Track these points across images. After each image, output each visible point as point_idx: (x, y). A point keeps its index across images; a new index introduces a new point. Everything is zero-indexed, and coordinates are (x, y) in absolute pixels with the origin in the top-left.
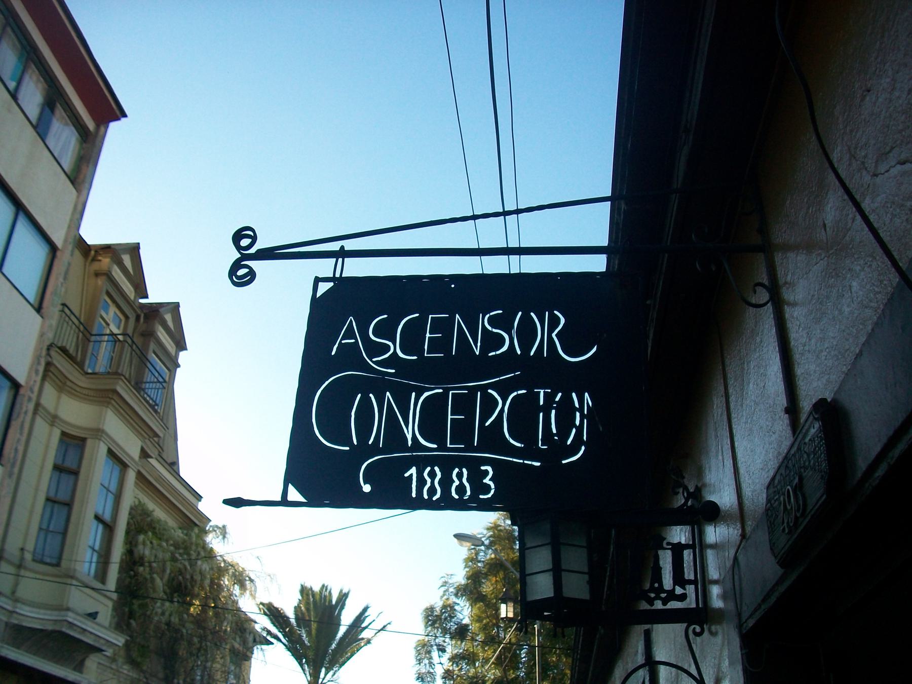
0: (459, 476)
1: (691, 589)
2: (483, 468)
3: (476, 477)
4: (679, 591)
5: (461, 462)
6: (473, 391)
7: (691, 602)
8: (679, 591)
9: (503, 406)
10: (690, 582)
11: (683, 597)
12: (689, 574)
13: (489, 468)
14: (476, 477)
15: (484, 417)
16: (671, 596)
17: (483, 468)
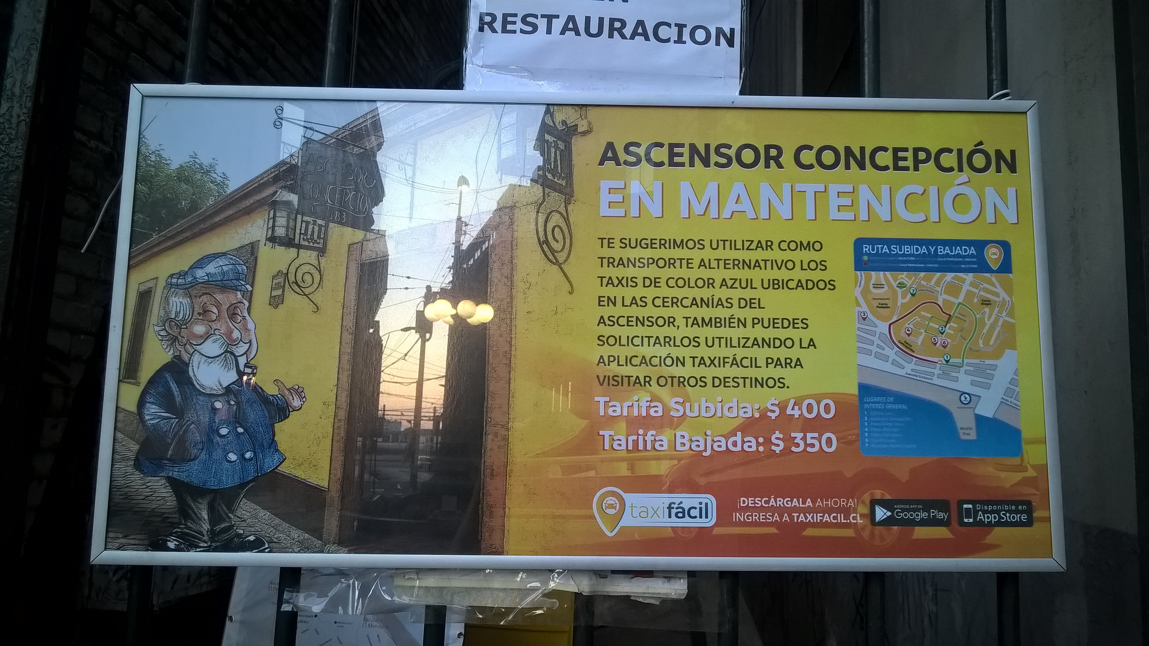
4: (318, 241)
7: (321, 246)
8: (318, 241)
11: (319, 243)
12: (322, 236)
16: (316, 242)
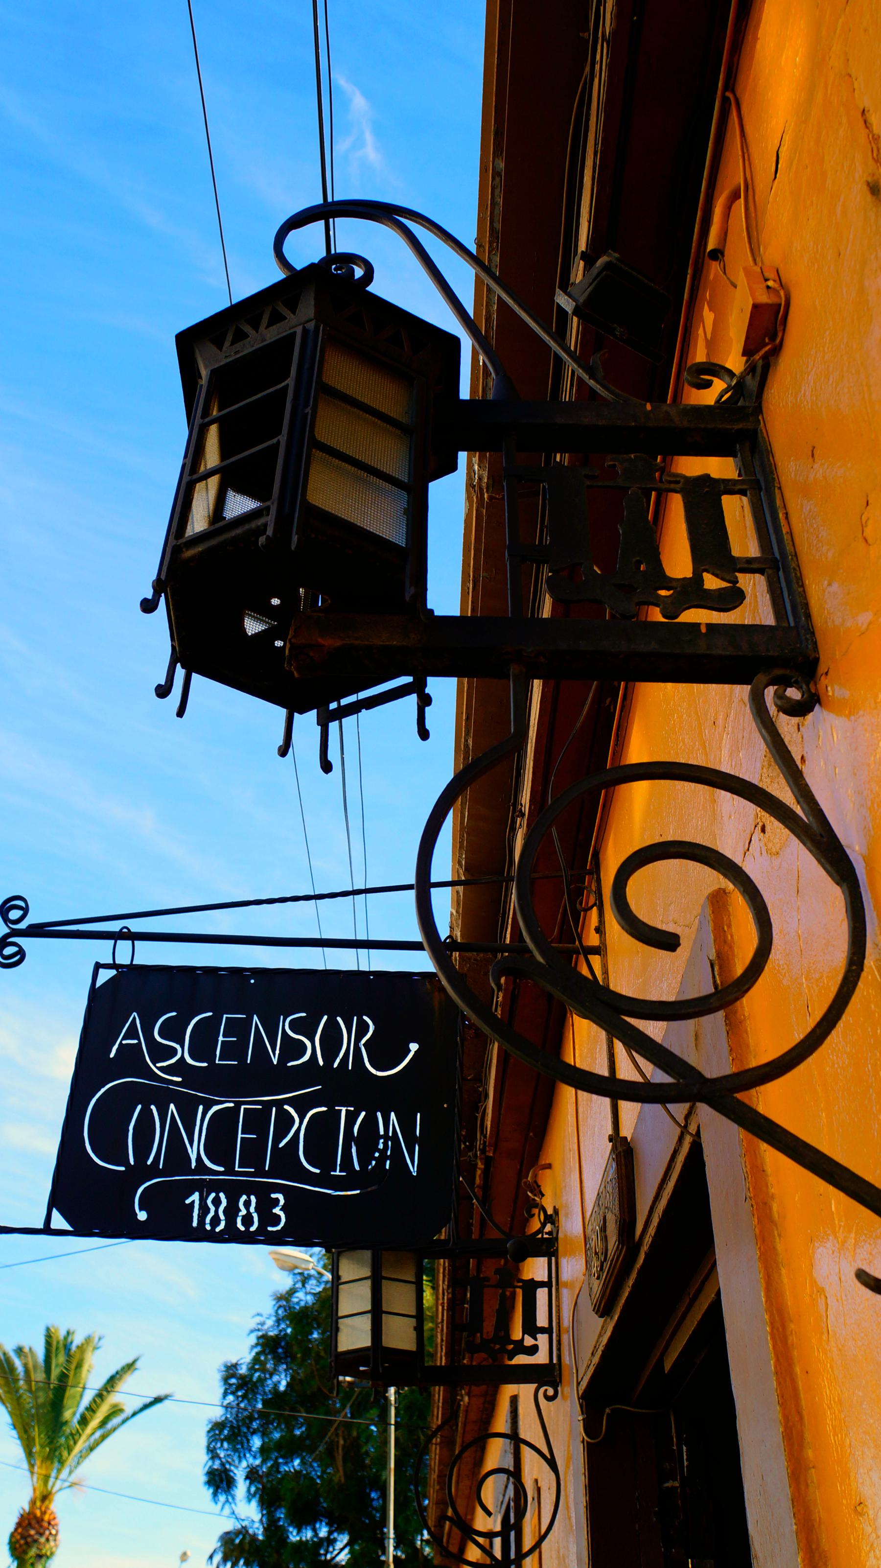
0: (247, 1204)
1: (542, 1340)
2: (273, 1196)
3: (265, 1207)
4: (529, 1341)
5: (249, 1188)
6: (268, 1105)
7: (541, 1358)
8: (529, 1341)
9: (300, 1125)
10: (543, 1330)
11: (533, 1350)
12: (542, 1320)
13: (280, 1197)
14: (265, 1207)
15: (278, 1138)
17: (273, 1196)
